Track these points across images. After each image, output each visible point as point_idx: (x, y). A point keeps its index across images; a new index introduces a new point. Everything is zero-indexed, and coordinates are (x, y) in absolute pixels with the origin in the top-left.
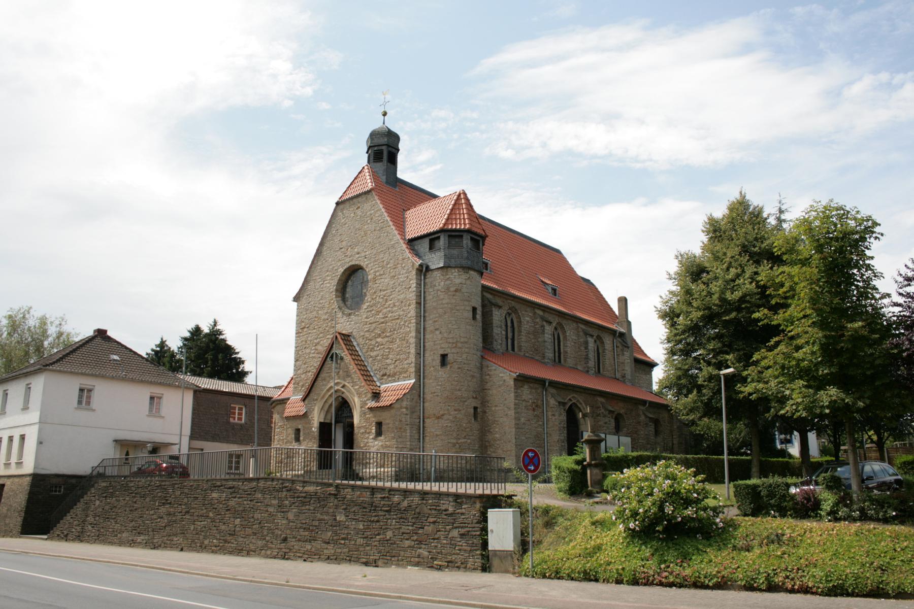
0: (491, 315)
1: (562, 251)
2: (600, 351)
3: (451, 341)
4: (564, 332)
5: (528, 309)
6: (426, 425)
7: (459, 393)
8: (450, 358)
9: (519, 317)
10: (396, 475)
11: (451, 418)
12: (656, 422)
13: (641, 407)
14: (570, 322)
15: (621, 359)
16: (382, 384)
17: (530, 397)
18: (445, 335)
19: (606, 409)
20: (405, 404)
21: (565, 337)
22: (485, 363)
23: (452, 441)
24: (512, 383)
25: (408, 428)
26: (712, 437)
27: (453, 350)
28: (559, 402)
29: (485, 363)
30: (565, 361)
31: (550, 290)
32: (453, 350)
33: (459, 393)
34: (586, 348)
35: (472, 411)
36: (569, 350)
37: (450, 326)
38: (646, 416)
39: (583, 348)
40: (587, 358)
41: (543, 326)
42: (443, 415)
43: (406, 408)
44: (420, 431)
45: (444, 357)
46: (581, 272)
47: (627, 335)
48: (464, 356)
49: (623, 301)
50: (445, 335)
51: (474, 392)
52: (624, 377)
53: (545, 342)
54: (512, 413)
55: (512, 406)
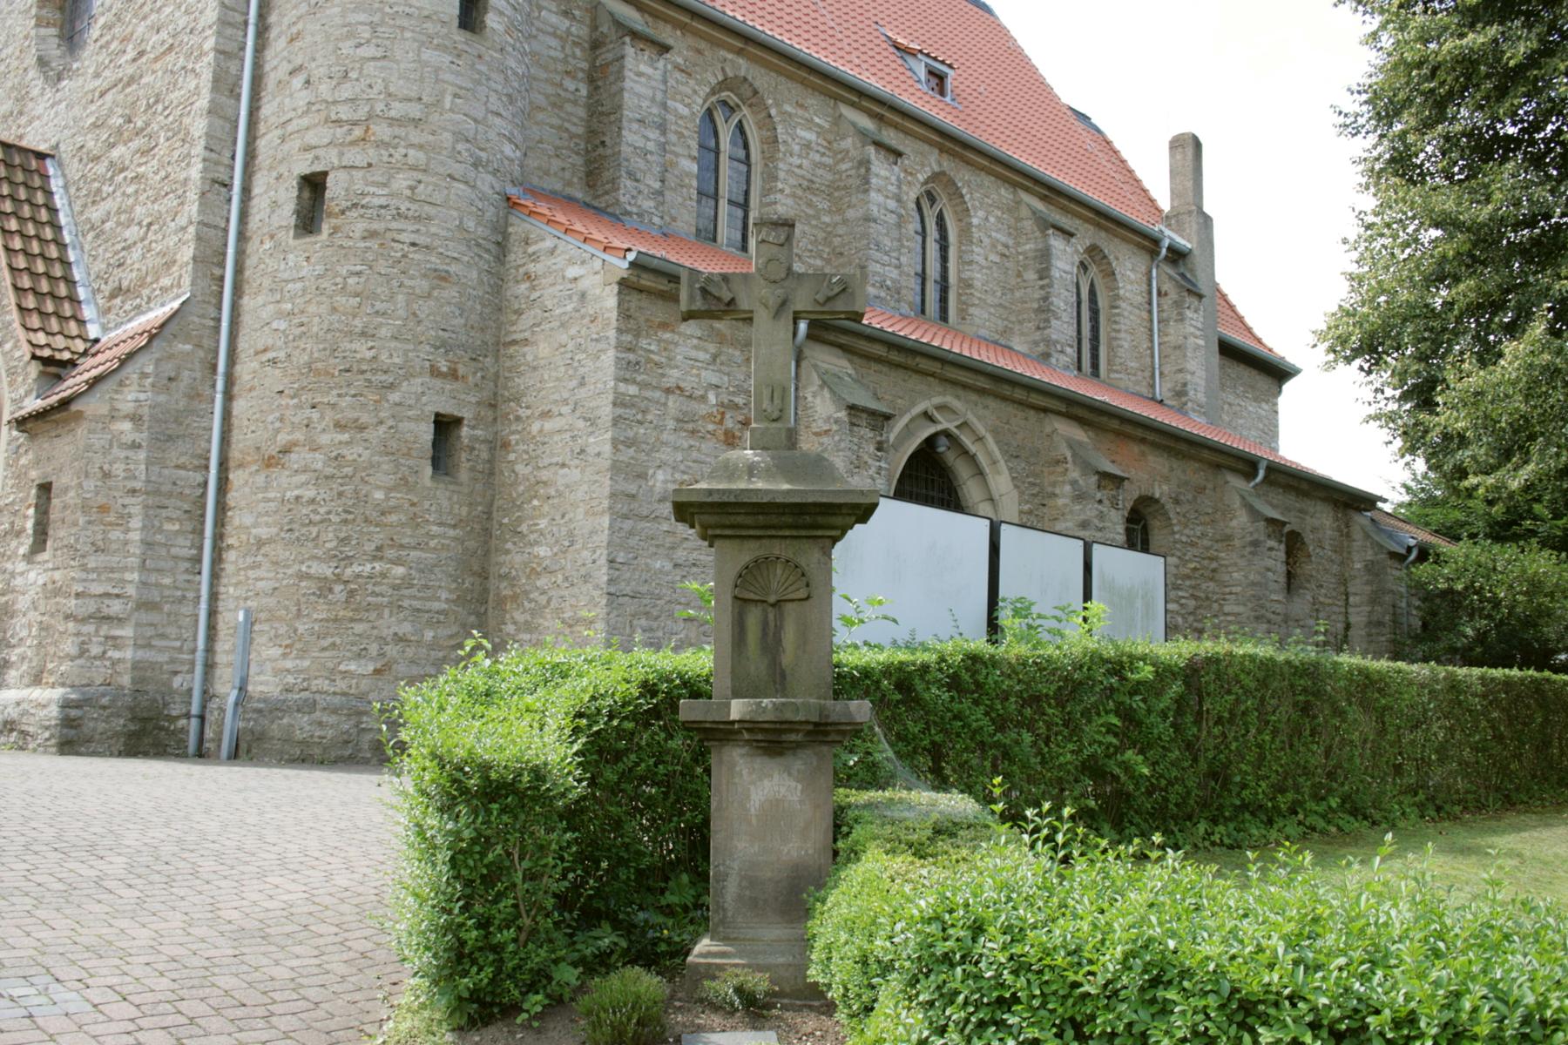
0: (620, 77)
1: (997, 11)
2: (1102, 303)
3: (345, 113)
4: (964, 213)
5: (813, 101)
6: (232, 498)
7: (363, 349)
8: (335, 188)
9: (768, 122)
10: (67, 722)
11: (318, 461)
12: (1294, 544)
13: (1236, 482)
14: (988, 180)
15: (1174, 333)
16: (105, 329)
17: (710, 376)
18: (324, 89)
19: (1086, 467)
20: (130, 396)
21: (965, 232)
22: (519, 226)
23: (317, 569)
24: (611, 302)
25: (136, 506)
26: (1496, 603)
27: (355, 156)
28: (852, 408)
29: (519, 226)
30: (963, 315)
31: (922, 73)
32: (355, 156)
33: (363, 349)
34: (1044, 273)
35: (426, 432)
36: (978, 277)
37: (347, 48)
38: (1254, 513)
39: (1031, 275)
40: (1045, 309)
41: (865, 163)
42: (285, 451)
43: (135, 418)
44: (196, 513)
45: (314, 185)
46: (1070, 93)
47: (1198, 259)
48: (401, 182)
49: (1188, 150)
50: (324, 89)
51: (443, 346)
52: (1180, 393)
53: (868, 219)
54: (601, 442)
55: (606, 411)
